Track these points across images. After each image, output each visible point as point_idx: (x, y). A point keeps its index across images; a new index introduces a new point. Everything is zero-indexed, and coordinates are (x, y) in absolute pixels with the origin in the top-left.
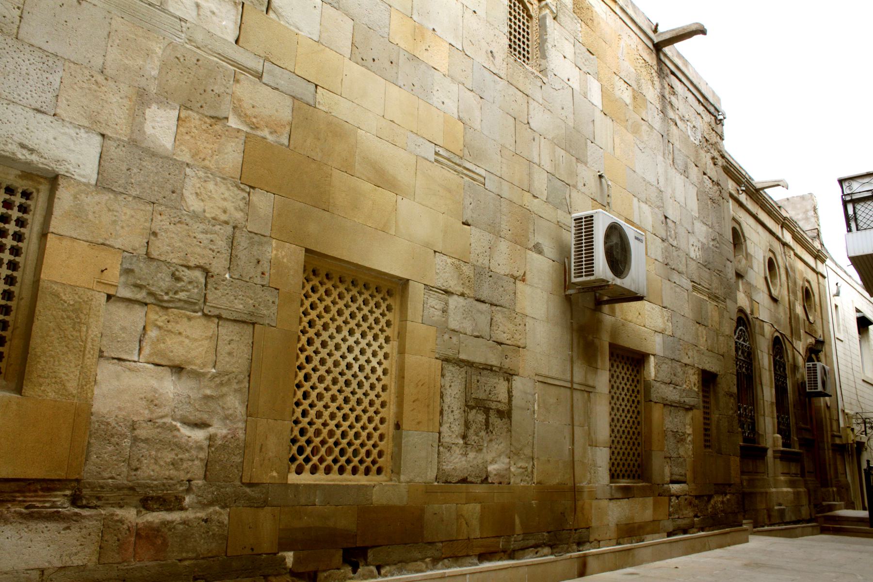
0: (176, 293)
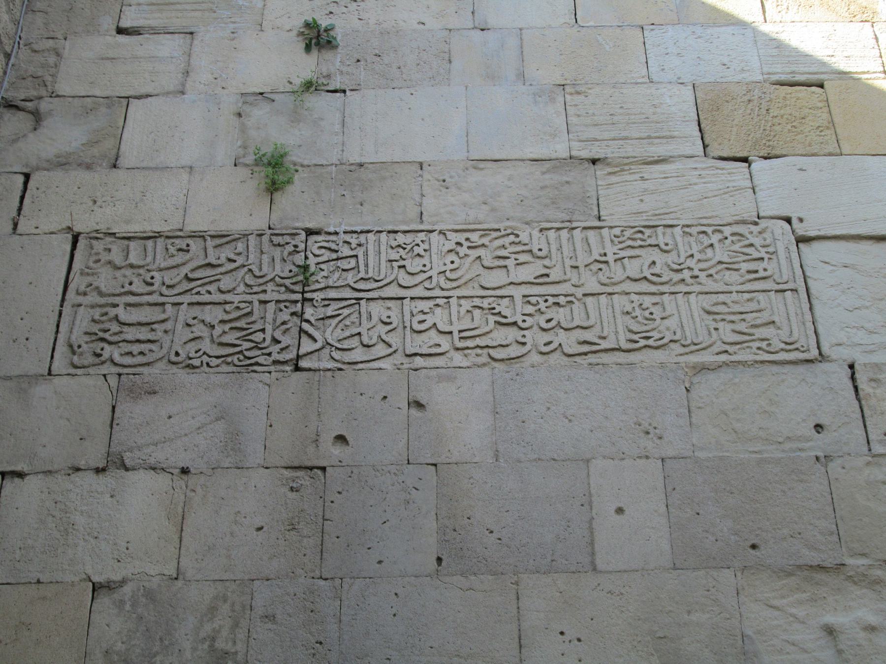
0: (139, 449)
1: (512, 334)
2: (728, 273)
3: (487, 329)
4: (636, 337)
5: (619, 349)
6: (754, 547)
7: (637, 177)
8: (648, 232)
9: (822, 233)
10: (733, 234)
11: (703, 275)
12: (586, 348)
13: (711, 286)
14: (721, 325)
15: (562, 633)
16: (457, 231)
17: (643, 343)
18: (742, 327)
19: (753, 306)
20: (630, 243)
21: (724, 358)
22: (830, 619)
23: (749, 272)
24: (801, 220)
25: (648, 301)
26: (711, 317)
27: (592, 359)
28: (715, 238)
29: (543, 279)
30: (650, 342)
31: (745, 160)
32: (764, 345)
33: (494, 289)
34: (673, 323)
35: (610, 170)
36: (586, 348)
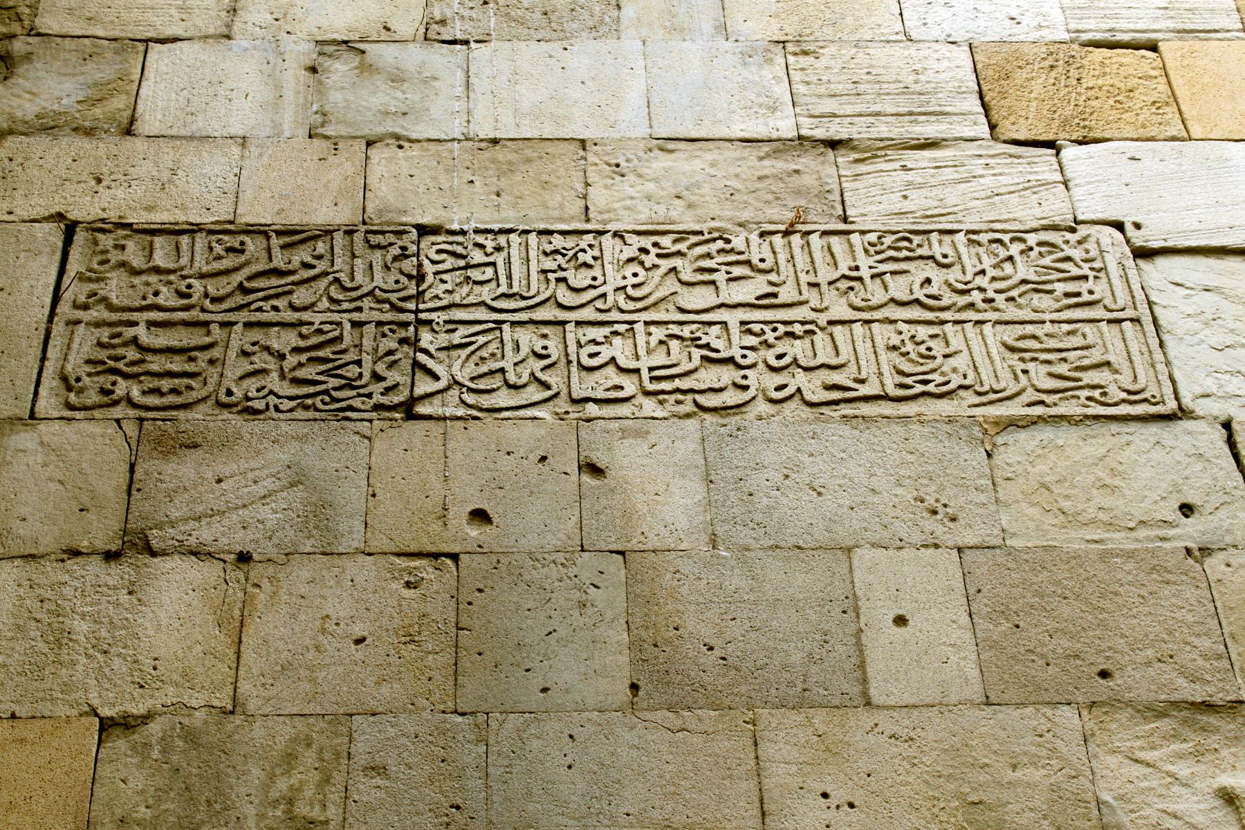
1: (727, 375)
2: (1036, 296)
3: (690, 366)
4: (909, 381)
5: (886, 397)
6: (1104, 674)
7: (897, 165)
8: (917, 240)
9: (1169, 244)
10: (1040, 244)
11: (1000, 298)
12: (836, 395)
13: (1012, 313)
14: (1031, 366)
15: (825, 795)
16: (639, 233)
17: (919, 388)
18: (1062, 369)
19: (1076, 341)
20: (892, 253)
21: (1039, 410)
22: (1226, 780)
23: (1067, 295)
24: (1138, 226)
25: (922, 332)
26: (1016, 356)
27: (847, 410)
28: (1015, 249)
29: (767, 301)
30: (931, 388)
31: (1050, 144)
32: (1096, 394)
33: (697, 312)
34: (961, 362)
35: (857, 156)
36: (836, 395)
